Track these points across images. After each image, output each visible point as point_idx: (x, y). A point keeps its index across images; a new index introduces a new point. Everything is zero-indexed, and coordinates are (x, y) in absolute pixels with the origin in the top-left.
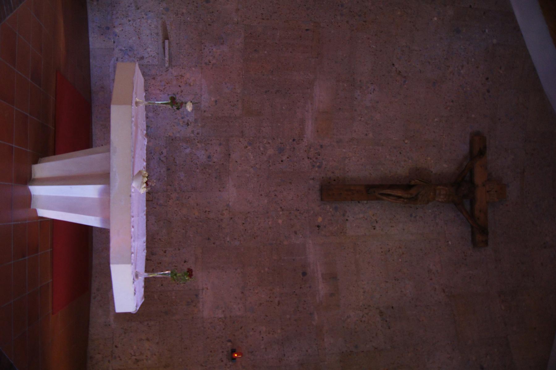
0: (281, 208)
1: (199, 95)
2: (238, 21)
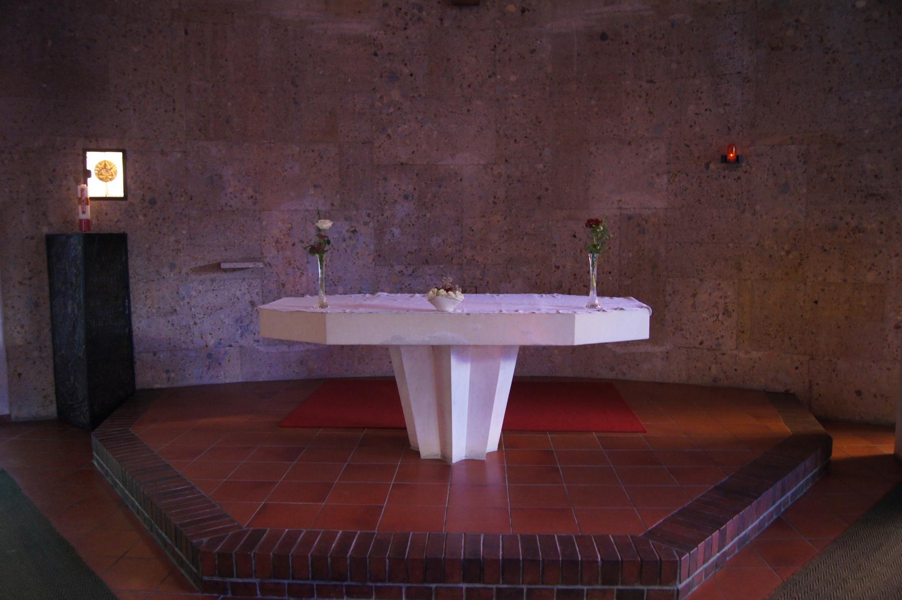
0: (490, 77)
1: (307, 214)
2: (181, 152)
